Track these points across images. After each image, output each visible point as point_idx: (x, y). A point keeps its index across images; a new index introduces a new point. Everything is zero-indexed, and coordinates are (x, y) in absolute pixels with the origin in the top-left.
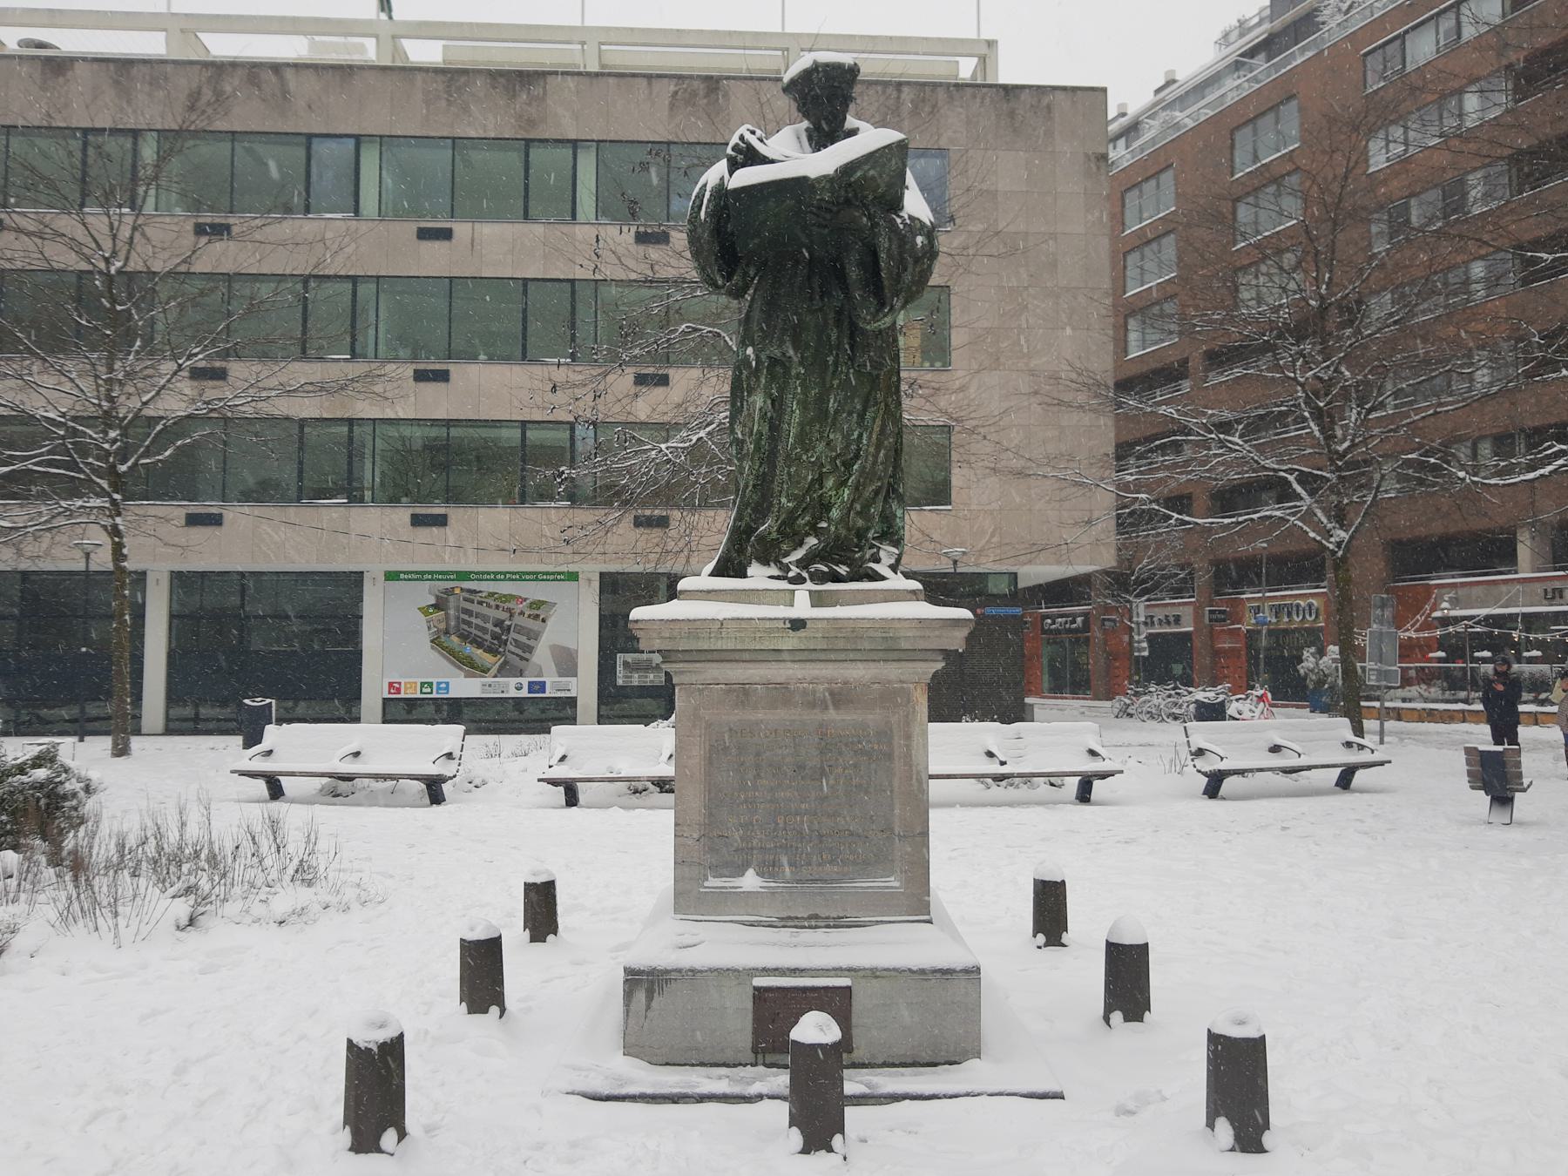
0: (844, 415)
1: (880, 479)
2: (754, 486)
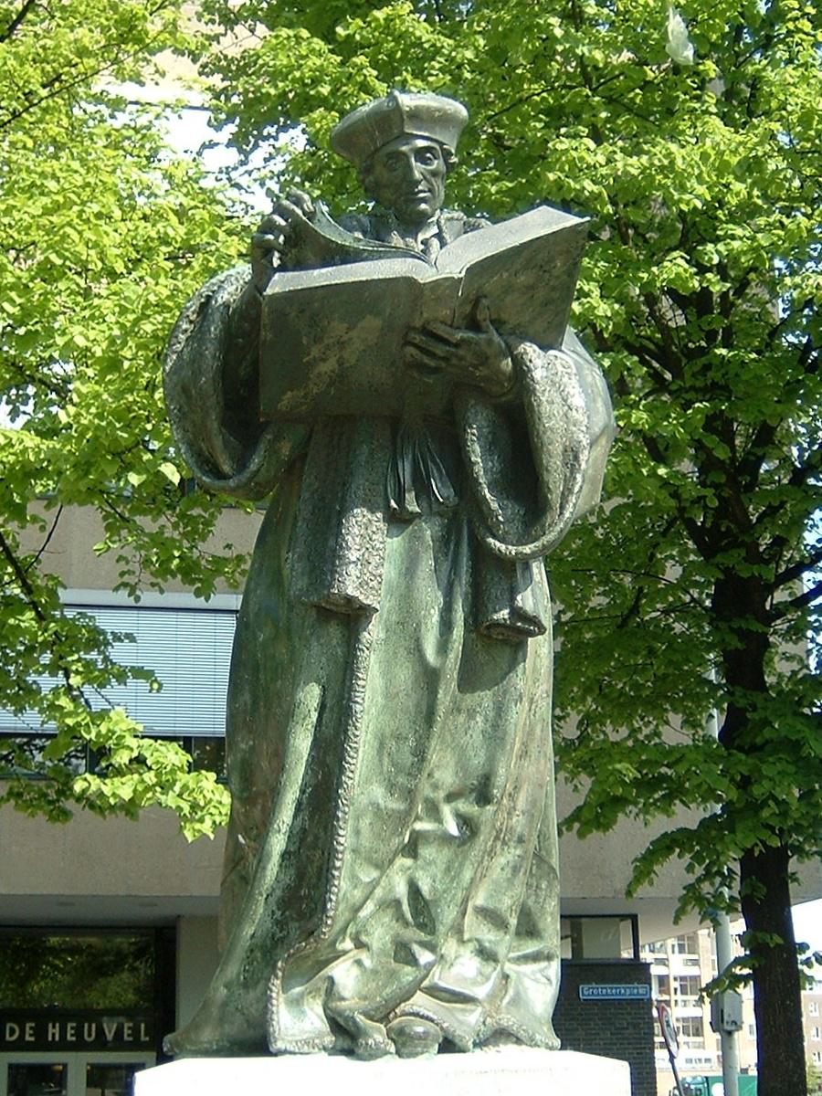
0: (462, 718)
1: (521, 840)
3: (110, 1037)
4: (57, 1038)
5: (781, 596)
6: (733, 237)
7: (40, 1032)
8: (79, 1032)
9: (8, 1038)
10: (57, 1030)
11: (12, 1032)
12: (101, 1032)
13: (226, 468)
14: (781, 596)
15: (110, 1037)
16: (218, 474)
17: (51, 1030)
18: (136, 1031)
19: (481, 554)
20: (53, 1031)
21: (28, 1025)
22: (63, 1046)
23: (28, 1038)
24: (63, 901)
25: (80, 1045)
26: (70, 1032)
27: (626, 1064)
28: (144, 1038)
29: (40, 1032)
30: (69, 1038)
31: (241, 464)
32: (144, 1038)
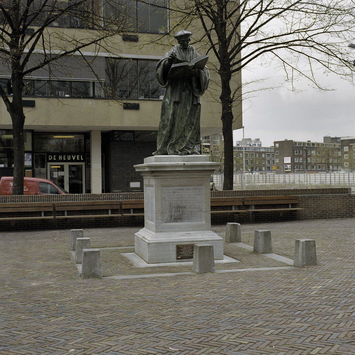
2: (169, 131)
3: (74, 159)
4: (61, 159)
5: (234, 68)
6: (245, 291)
7: (57, 158)
8: (66, 158)
9: (50, 159)
10: (61, 157)
11: (50, 158)
12: (71, 158)
13: (163, 85)
14: (234, 68)
15: (74, 159)
16: (162, 85)
17: (60, 157)
18: (80, 158)
19: (193, 95)
20: (60, 158)
21: (54, 156)
22: (63, 161)
23: (54, 159)
24: (65, 127)
25: (67, 161)
26: (64, 158)
27: (145, 159)
28: (82, 159)
29: (57, 158)
30: (64, 159)
31: (165, 84)
32: (82, 159)
